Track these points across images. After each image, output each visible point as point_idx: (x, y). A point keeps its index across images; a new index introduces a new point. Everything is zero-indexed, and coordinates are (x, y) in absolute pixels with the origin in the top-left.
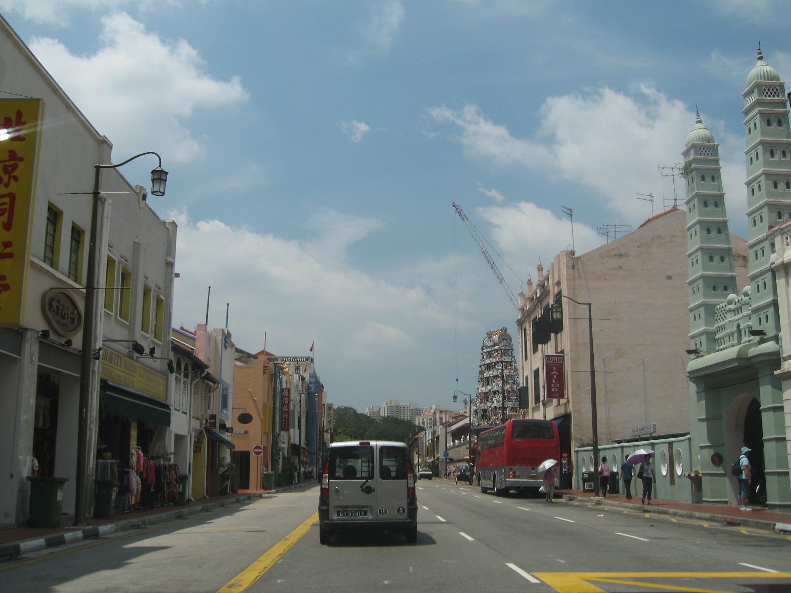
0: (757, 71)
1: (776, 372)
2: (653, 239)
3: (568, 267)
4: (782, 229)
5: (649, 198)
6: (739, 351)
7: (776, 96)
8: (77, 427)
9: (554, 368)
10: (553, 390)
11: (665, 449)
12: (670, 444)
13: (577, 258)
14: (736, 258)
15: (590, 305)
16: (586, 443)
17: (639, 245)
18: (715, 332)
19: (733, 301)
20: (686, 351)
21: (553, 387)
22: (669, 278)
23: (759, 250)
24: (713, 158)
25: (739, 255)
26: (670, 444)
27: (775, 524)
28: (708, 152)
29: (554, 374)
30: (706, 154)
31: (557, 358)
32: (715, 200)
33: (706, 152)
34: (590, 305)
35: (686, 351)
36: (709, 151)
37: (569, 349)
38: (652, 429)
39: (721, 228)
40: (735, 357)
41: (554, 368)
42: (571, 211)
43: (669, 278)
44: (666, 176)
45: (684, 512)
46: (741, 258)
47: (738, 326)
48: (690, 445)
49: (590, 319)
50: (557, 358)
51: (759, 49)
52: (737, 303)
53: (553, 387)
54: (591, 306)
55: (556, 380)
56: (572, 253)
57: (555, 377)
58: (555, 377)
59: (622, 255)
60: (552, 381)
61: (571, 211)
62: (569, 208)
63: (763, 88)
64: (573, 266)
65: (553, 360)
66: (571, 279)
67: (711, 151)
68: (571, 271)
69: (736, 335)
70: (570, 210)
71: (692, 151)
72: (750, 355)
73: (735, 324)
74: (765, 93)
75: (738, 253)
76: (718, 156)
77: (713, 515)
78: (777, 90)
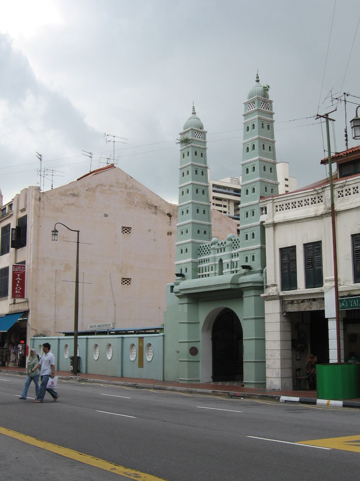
0: (254, 91)
1: (262, 295)
2: (97, 186)
3: (36, 199)
4: (273, 200)
5: (89, 155)
6: (232, 278)
7: (267, 109)
8: (341, 346)
9: (19, 276)
10: (16, 292)
11: (136, 342)
12: (141, 339)
13: (43, 193)
15: (78, 232)
16: (39, 333)
17: (87, 189)
18: (197, 262)
19: (217, 243)
20: (176, 274)
21: (17, 290)
22: (106, 215)
23: (250, 211)
24: (203, 141)
25: (152, 205)
26: (141, 339)
27: (280, 397)
28: (200, 136)
29: (18, 280)
30: (199, 137)
31: (21, 268)
32: (196, 169)
33: (199, 135)
34: (78, 232)
35: (176, 274)
36: (201, 135)
37: (31, 261)
38: (112, 326)
39: (205, 191)
40: (230, 282)
41: (19, 276)
42: (41, 157)
43: (106, 215)
44: (108, 135)
45: (184, 389)
46: (153, 207)
47: (221, 261)
48: (164, 340)
49: (78, 243)
50: (21, 268)
51: (257, 75)
52: (220, 245)
53: (17, 290)
54: (79, 232)
55: (19, 284)
56: (39, 189)
57: (18, 282)
58: (18, 282)
59: (75, 195)
60: (16, 285)
61: (41, 157)
62: (40, 154)
63: (261, 102)
64: (40, 199)
65: (18, 269)
66: (38, 209)
67: (202, 135)
68: (38, 202)
69: (218, 266)
70: (40, 155)
71: (190, 132)
72: (240, 282)
73: (218, 260)
75: (152, 204)
76: (206, 140)
77: (133, 383)
78: (268, 105)
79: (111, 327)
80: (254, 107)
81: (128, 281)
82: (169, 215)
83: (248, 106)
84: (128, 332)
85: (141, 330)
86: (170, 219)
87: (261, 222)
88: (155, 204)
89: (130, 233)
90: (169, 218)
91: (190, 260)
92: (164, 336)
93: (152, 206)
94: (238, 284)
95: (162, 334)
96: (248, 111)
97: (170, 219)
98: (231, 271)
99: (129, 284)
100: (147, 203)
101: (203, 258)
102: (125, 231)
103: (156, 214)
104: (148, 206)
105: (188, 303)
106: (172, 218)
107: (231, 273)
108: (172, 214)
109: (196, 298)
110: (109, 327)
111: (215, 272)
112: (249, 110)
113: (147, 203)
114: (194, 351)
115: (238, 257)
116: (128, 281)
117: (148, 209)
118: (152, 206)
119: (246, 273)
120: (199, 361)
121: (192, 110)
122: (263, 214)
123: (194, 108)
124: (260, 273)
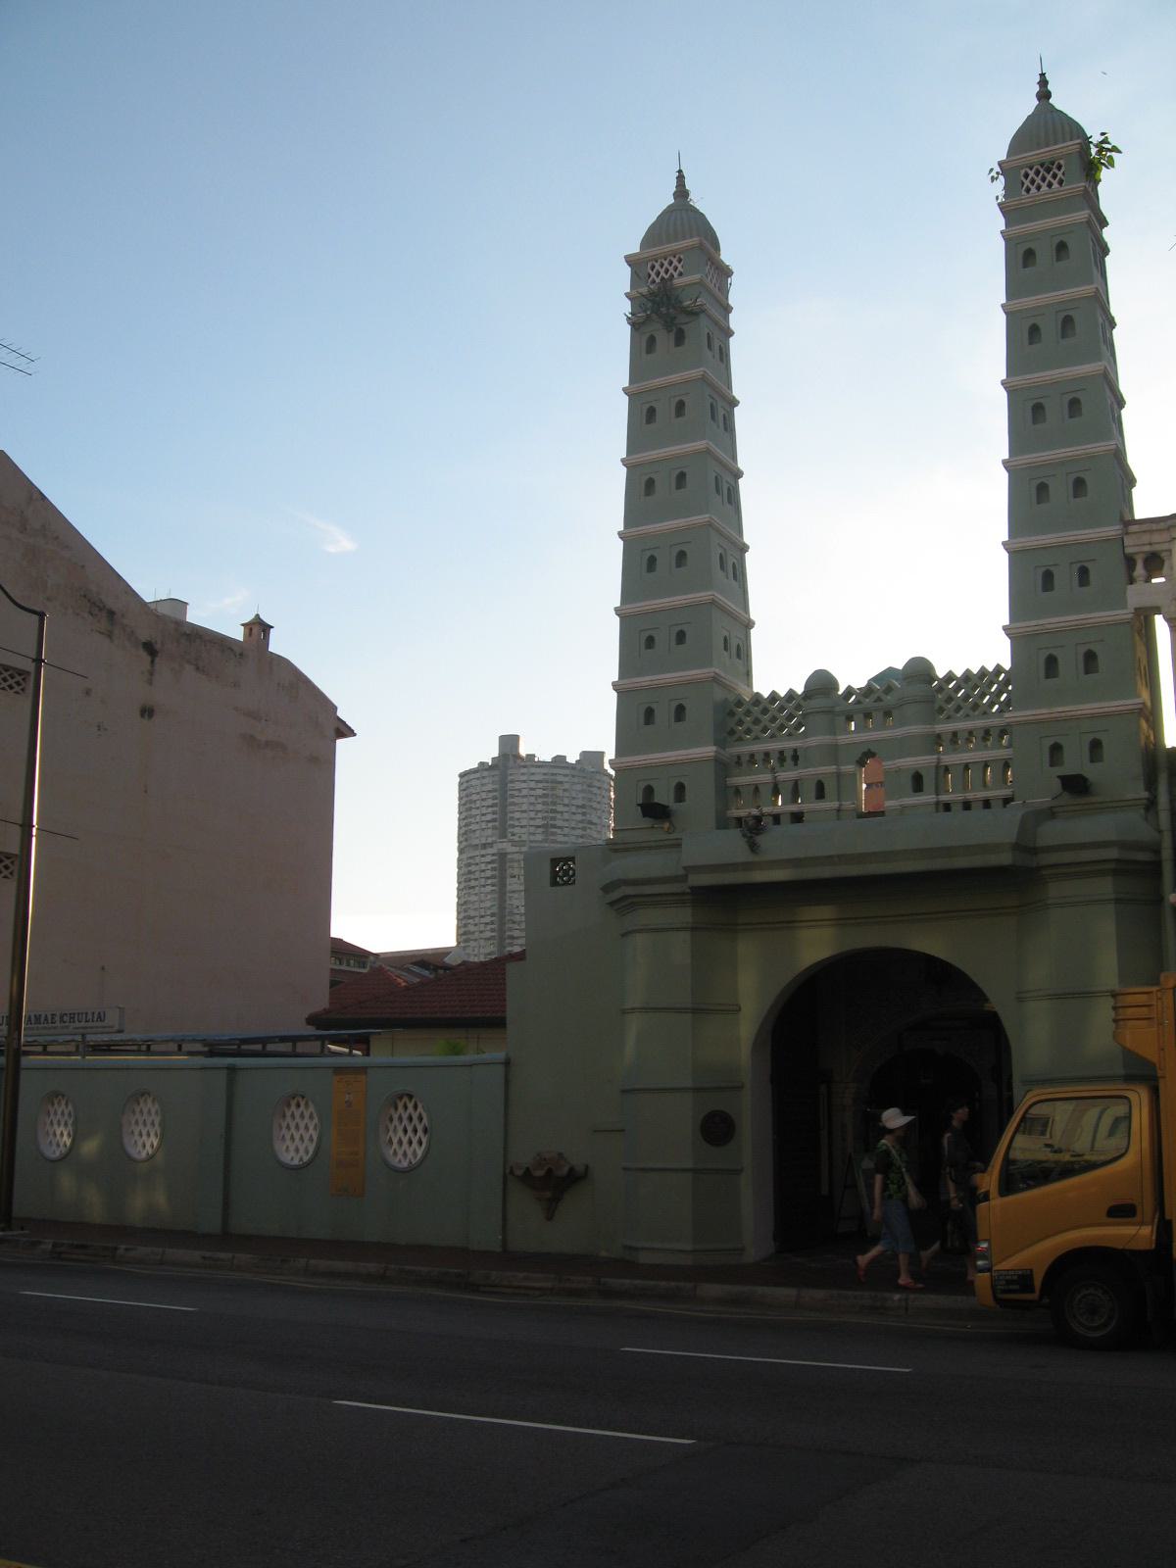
14: (96, 611)
15: (42, 615)
40: (1014, 841)
48: (507, 1082)
74: (1027, 183)
79: (112, 1027)
80: (1061, 182)
81: (7, 862)
82: (150, 648)
83: (1026, 176)
84: (113, 1048)
85: (245, 1041)
86: (152, 662)
87: (1136, 609)
88: (110, 603)
89: (23, 690)
90: (149, 658)
91: (709, 750)
92: (507, 1063)
93: (100, 610)
94: (1034, 851)
95: (501, 1056)
96: (1024, 193)
97: (152, 662)
98: (937, 803)
99: (9, 876)
100: (85, 596)
101: (745, 749)
102: (8, 683)
103: (110, 635)
104: (88, 605)
105: (693, 929)
106: (157, 660)
107: (937, 811)
108: (158, 647)
109: (725, 904)
110: (100, 1024)
111: (841, 805)
112: (1028, 190)
113: (85, 596)
114: (717, 1128)
115: (796, 764)
116: (7, 862)
117: (86, 615)
118: (100, 610)
119: (1055, 810)
120: (738, 1172)
121: (674, 183)
122: (1132, 581)
123: (681, 177)
124: (1142, 811)
